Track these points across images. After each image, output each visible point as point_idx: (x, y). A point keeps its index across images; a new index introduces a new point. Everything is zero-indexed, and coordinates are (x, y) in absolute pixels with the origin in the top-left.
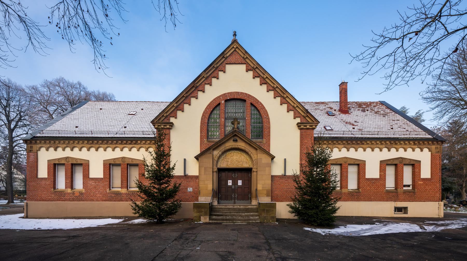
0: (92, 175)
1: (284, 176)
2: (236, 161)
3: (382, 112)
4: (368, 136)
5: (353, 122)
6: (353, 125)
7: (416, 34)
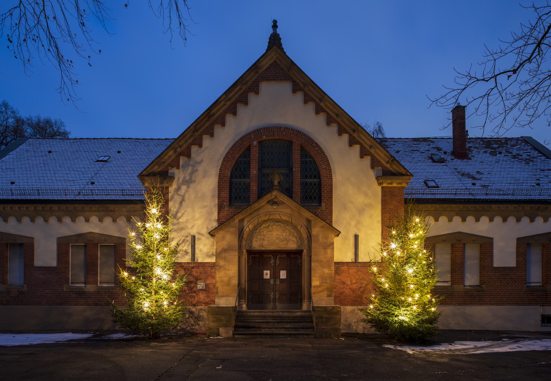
0: (38, 262)
1: (356, 262)
2: (277, 238)
3: (524, 156)
4: (497, 197)
5: (473, 172)
6: (474, 178)
7: (514, 73)
